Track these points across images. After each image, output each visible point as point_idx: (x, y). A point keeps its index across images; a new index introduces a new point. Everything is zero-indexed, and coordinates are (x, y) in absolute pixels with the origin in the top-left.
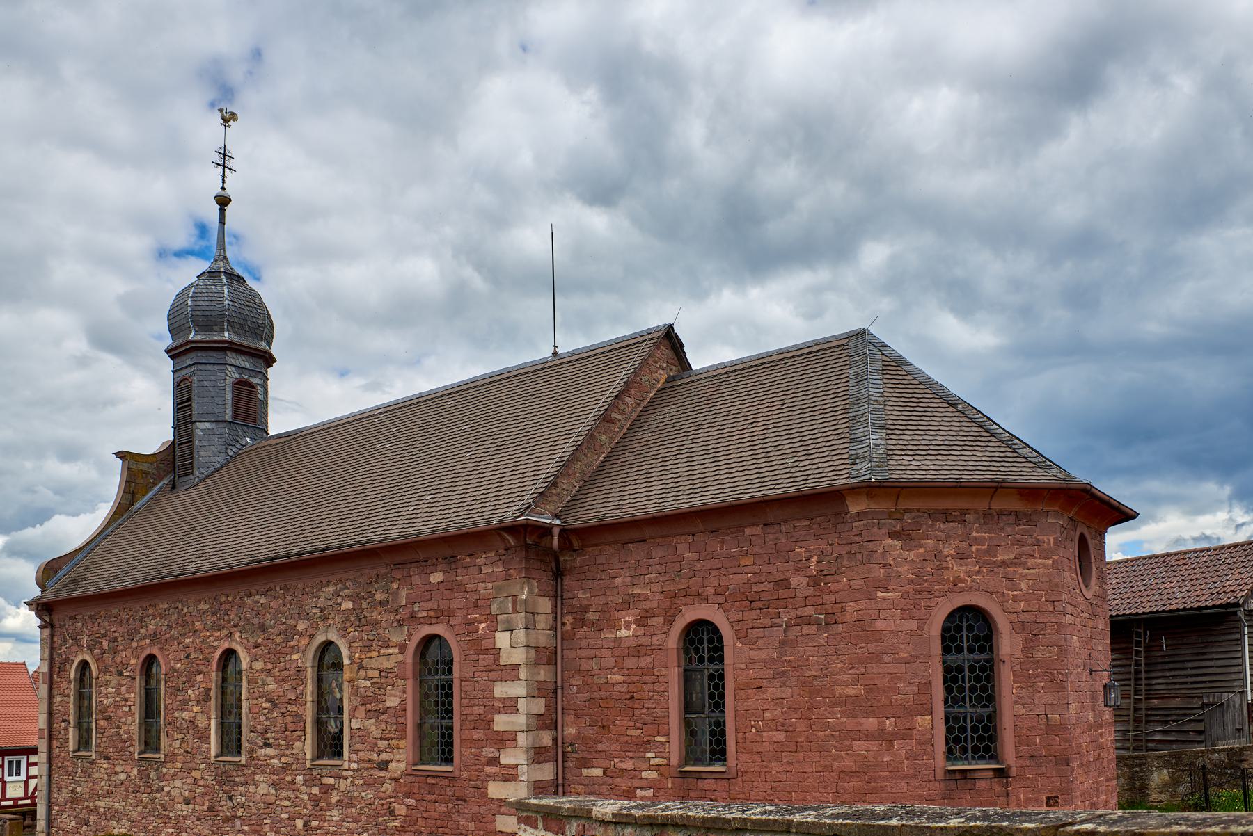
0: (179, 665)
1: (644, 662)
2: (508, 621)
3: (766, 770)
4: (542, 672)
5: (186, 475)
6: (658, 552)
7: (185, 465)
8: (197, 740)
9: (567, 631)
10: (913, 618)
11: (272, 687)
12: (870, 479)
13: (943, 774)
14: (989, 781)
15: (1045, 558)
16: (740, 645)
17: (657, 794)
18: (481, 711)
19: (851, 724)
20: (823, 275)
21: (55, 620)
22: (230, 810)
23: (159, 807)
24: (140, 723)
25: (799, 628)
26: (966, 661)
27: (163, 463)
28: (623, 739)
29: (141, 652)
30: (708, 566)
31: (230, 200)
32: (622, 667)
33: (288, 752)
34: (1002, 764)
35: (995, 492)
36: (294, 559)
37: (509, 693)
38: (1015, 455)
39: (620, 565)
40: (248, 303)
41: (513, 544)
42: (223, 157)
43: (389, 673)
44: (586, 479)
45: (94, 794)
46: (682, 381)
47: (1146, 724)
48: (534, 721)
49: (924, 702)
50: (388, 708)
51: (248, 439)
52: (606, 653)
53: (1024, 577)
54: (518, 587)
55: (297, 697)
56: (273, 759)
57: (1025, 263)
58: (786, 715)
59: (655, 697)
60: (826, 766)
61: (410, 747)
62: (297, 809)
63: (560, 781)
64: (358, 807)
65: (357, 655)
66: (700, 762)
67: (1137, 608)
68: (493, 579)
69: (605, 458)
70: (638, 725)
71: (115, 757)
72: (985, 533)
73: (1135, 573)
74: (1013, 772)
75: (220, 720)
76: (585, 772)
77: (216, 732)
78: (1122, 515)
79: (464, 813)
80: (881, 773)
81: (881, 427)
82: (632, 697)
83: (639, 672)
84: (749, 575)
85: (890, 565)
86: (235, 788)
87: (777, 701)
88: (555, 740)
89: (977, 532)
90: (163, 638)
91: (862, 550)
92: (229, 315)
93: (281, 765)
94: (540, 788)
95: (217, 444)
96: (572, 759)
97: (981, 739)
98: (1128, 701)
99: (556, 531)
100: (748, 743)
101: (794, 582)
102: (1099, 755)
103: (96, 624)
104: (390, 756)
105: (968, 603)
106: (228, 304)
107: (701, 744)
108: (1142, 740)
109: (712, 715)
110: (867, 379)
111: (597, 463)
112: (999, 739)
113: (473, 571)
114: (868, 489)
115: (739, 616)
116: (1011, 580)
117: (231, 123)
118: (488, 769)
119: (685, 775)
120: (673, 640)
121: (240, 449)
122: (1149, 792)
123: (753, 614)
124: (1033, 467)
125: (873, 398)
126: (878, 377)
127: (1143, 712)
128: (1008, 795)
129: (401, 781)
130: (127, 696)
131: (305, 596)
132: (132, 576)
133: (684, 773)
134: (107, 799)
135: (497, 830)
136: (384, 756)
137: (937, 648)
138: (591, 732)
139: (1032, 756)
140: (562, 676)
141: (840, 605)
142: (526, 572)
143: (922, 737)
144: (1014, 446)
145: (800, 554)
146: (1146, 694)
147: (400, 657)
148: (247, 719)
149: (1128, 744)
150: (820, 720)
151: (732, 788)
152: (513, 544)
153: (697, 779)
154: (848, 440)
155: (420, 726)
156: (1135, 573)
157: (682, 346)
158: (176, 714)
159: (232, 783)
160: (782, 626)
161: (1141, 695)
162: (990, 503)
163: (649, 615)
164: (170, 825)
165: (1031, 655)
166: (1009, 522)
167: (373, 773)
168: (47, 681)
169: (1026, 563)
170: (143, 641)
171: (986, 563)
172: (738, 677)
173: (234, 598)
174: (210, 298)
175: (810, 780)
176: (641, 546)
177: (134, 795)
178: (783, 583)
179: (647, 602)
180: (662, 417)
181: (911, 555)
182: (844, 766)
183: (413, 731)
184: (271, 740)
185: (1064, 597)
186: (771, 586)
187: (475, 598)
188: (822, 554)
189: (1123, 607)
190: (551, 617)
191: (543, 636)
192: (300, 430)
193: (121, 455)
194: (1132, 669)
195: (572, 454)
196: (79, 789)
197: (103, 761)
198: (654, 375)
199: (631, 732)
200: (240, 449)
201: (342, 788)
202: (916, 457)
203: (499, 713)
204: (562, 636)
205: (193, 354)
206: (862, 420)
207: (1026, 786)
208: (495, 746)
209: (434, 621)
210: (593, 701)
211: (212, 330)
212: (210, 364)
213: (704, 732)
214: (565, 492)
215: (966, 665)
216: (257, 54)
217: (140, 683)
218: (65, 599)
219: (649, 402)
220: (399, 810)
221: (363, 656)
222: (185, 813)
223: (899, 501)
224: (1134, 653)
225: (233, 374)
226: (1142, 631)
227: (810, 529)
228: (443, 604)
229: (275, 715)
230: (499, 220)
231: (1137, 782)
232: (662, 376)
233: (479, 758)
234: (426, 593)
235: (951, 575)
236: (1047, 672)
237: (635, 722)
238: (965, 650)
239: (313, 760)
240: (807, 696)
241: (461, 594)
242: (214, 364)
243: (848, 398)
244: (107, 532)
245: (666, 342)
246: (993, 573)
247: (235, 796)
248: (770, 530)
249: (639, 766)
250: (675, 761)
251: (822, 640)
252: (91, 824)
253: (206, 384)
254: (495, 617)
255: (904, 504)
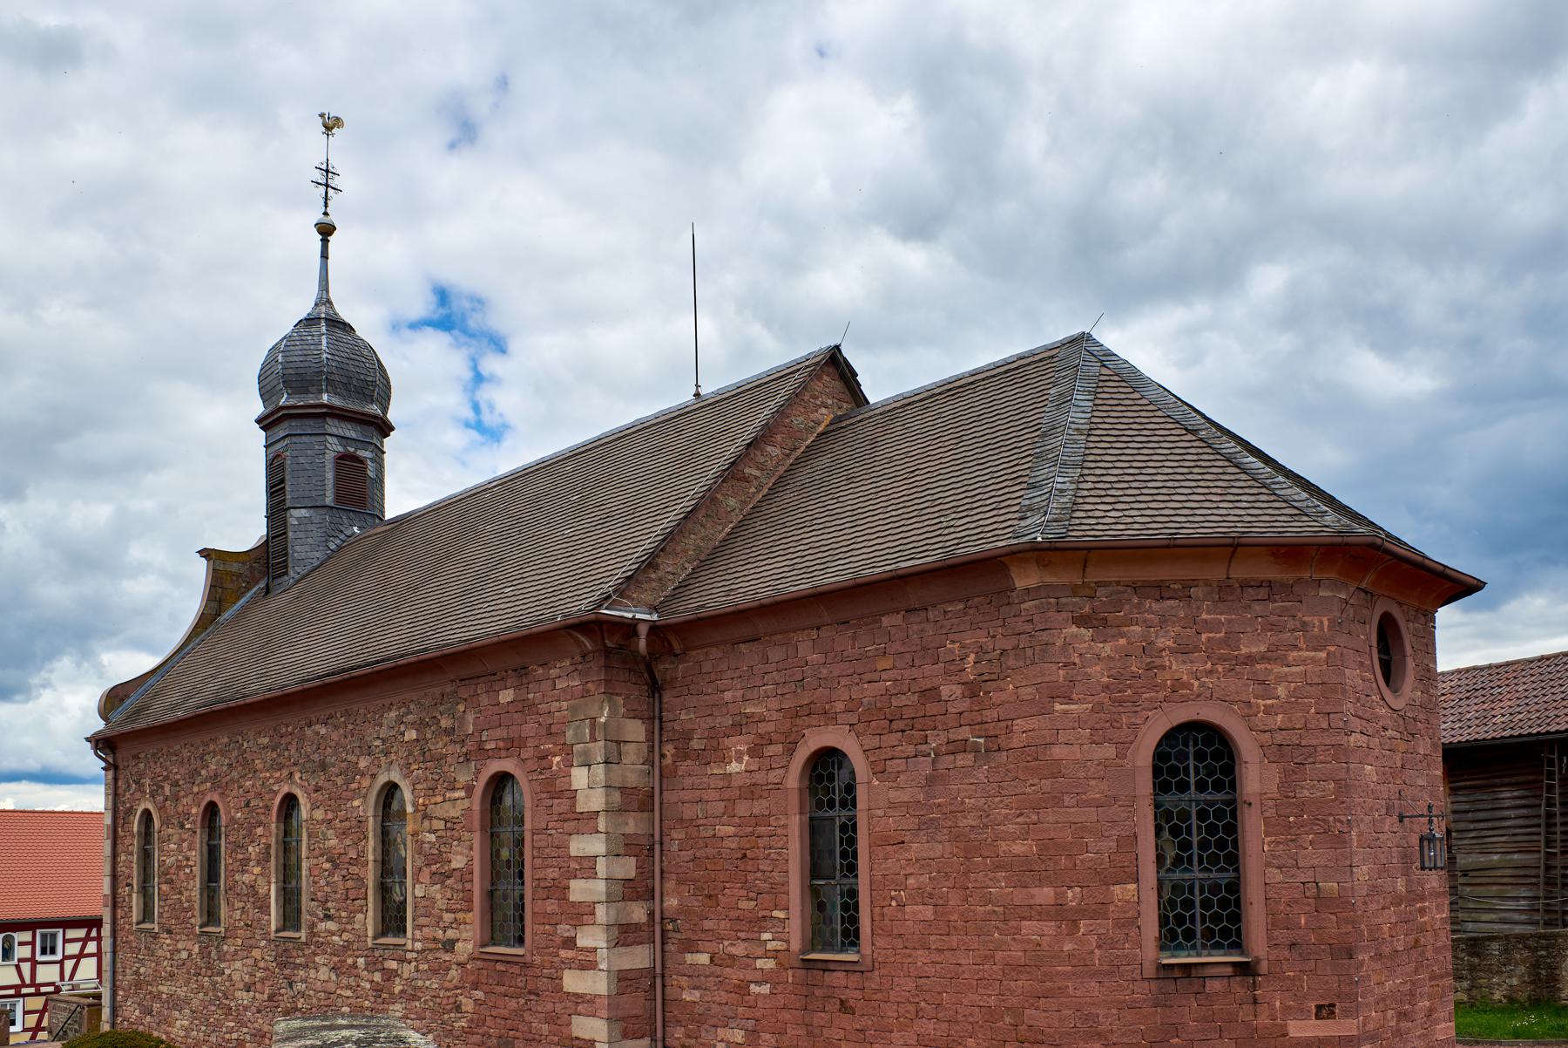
0: (239, 814)
1: (759, 807)
2: (586, 753)
3: (910, 960)
4: (631, 822)
5: (280, 576)
6: (776, 654)
7: (279, 563)
8: (257, 910)
9: (667, 766)
10: (1110, 741)
11: (333, 842)
12: (1036, 538)
13: (1154, 971)
14: (1226, 981)
15: (1315, 650)
16: (877, 783)
17: (775, 991)
18: (556, 875)
19: (1019, 896)
20: (1201, 309)
21: (119, 761)
22: (291, 1000)
23: (220, 994)
24: (201, 889)
25: (952, 757)
26: (1194, 804)
27: (259, 563)
28: (734, 914)
29: (202, 799)
30: (836, 673)
31: (335, 229)
32: (732, 814)
33: (349, 927)
34: (1247, 956)
35: (1234, 552)
36: (346, 676)
37: (586, 850)
38: (1273, 498)
39: (730, 674)
40: (352, 356)
41: (590, 648)
42: (325, 174)
43: (454, 823)
44: (702, 558)
45: (157, 978)
46: (848, 422)
47: (1563, 888)
48: (618, 889)
49: (1126, 864)
50: (454, 870)
51: (355, 529)
52: (713, 795)
53: (1282, 678)
54: (596, 706)
55: (359, 856)
56: (334, 935)
57: (1470, 281)
58: (935, 882)
59: (772, 855)
60: (986, 956)
61: (477, 921)
62: (358, 1000)
63: (658, 970)
64: (422, 1000)
65: (421, 800)
66: (830, 948)
67: (1548, 724)
68: (569, 697)
69: (733, 529)
70: (752, 895)
71: (177, 931)
72: (1221, 614)
73: (1550, 676)
74: (1264, 967)
75: (281, 884)
76: (689, 958)
77: (277, 900)
78: (1458, 587)
79: (536, 1012)
80: (1060, 968)
81: (1074, 466)
82: (745, 856)
83: (753, 822)
84: (888, 683)
85: (1075, 664)
86: (296, 972)
87: (924, 862)
88: (651, 914)
89: (1209, 613)
90: (224, 780)
91: (1033, 644)
92: (328, 372)
93: (341, 943)
94: (627, 979)
95: (316, 535)
96: (676, 941)
97: (1216, 918)
98: (1536, 856)
99: (643, 630)
100: (887, 921)
101: (945, 691)
102: (1417, 941)
103: (158, 765)
104: (456, 933)
105: (1196, 718)
106: (327, 358)
107: (831, 922)
108: (1557, 911)
109: (845, 881)
110: (1071, 400)
111: (720, 537)
112: (1244, 919)
113: (546, 685)
114: (1036, 553)
115: (875, 742)
116: (1263, 683)
117: (335, 130)
118: (563, 953)
119: (808, 965)
120: (793, 777)
121: (344, 541)
122: (1561, 986)
123: (893, 739)
124: (1296, 515)
125: (1073, 426)
126: (1089, 397)
127: (1558, 872)
128: (1255, 1002)
129: (468, 966)
130: (189, 853)
131: (367, 723)
132: (192, 703)
133: (807, 962)
134: (169, 983)
135: (574, 1035)
136: (451, 934)
137: (1145, 784)
138: (695, 903)
139: (1294, 944)
140: (661, 827)
141: (1004, 724)
142: (605, 685)
143: (1122, 916)
144: (1273, 486)
145: (952, 651)
146: (1562, 847)
147: (466, 803)
148: (308, 883)
149: (1537, 917)
150: (978, 891)
151: (866, 985)
152: (590, 648)
153: (824, 970)
154: (1025, 486)
155: (490, 895)
156: (1550, 676)
157: (855, 374)
158: (237, 877)
159: (292, 965)
160: (929, 755)
161: (1556, 847)
162: (1228, 570)
163: (765, 742)
164: (231, 1017)
165: (1293, 794)
166: (1259, 598)
167: (438, 955)
168: (111, 836)
169: (1285, 656)
170: (204, 785)
171: (1222, 659)
172: (874, 828)
173: (294, 729)
174: (305, 352)
175: (965, 976)
176: (754, 646)
177: (195, 978)
178: (930, 694)
179: (764, 724)
180: (813, 470)
181: (1107, 649)
182: (1009, 956)
183: (481, 901)
184: (331, 910)
185: (1349, 707)
186: (916, 698)
187: (548, 722)
188: (981, 650)
189: (1530, 723)
190: (645, 747)
191: (632, 771)
192: (410, 514)
193: (206, 553)
194: (1542, 811)
195: (678, 525)
196: (142, 970)
197: (165, 936)
198: (811, 416)
199: (744, 904)
200: (344, 541)
201: (405, 976)
202: (1117, 507)
203: (575, 877)
204: (661, 772)
205: (285, 424)
206: (1049, 456)
207: (1284, 988)
208: (570, 922)
209: (503, 753)
210: (698, 861)
211: (307, 392)
212: (307, 434)
213: (834, 905)
214: (671, 577)
215: (1194, 810)
216: (503, 83)
217: (201, 838)
218: (123, 734)
219: (803, 452)
220: (465, 1005)
221: (427, 802)
222: (245, 1002)
223: (1088, 570)
224: (1545, 788)
225: (334, 447)
226: (1555, 756)
227: (966, 614)
228: (514, 732)
229: (336, 878)
230: (792, 264)
231: (1543, 972)
232: (825, 416)
233: (553, 938)
234: (494, 717)
235: (1167, 677)
236: (1318, 819)
237: (749, 890)
238: (1193, 788)
239: (375, 938)
240: (961, 855)
241: (533, 717)
242: (311, 435)
243: (1040, 429)
244: (186, 650)
245: (831, 370)
246: (1233, 673)
247: (296, 982)
248: (914, 618)
249: (753, 951)
250: (796, 945)
251: (981, 775)
252: (154, 1013)
253: (302, 460)
254: (570, 748)
255: (1093, 575)
